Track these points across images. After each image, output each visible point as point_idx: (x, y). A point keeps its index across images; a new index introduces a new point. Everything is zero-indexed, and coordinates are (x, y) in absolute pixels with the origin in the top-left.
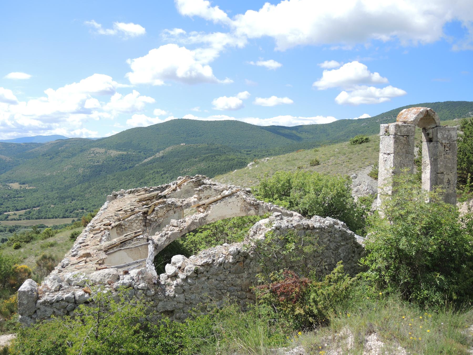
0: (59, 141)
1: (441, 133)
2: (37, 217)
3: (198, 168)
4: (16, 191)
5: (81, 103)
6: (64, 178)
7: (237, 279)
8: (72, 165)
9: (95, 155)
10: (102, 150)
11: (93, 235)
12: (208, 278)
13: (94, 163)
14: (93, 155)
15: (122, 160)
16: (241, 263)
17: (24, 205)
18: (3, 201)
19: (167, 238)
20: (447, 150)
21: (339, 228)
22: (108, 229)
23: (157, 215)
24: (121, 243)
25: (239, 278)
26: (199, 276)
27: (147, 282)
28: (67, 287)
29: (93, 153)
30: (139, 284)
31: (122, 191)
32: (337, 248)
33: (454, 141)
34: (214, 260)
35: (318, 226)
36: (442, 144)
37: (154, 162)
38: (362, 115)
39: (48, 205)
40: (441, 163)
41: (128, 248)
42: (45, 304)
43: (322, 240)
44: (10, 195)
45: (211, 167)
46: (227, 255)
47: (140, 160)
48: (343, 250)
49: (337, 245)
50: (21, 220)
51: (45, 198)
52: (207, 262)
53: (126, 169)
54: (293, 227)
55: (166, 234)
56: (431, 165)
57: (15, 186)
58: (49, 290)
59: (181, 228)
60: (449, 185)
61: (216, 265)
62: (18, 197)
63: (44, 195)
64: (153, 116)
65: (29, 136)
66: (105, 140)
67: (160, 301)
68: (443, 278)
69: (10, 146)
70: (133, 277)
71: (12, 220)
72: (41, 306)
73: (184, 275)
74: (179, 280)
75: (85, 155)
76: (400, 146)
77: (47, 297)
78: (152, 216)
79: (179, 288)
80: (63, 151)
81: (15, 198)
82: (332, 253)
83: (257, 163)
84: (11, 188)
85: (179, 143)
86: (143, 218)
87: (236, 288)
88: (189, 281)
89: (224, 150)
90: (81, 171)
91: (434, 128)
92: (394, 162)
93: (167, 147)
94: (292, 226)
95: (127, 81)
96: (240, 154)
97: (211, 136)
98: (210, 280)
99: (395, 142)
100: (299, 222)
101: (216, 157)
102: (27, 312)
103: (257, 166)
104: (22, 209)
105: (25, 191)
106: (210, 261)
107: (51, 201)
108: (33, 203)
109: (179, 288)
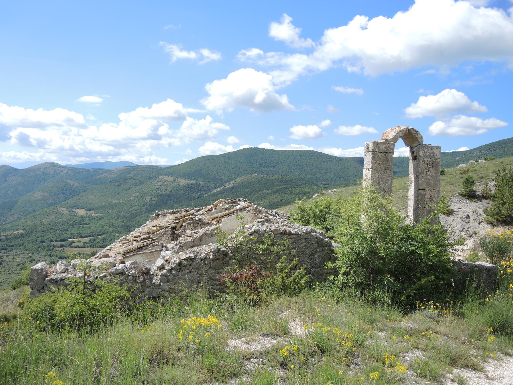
0: (127, 168)
1: (423, 151)
2: (101, 245)
3: (270, 201)
4: (82, 217)
5: (152, 128)
6: (130, 206)
7: (216, 274)
8: (140, 193)
9: (163, 183)
10: (171, 179)
11: (121, 244)
12: (191, 272)
13: (161, 191)
14: (161, 183)
15: (190, 189)
16: (221, 260)
17: (89, 232)
18: (68, 227)
19: (180, 247)
20: (429, 168)
21: (316, 235)
22: (138, 241)
23: (185, 230)
24: (138, 248)
25: (218, 273)
26: (182, 268)
27: (138, 271)
28: (72, 270)
29: (162, 181)
30: (131, 272)
31: (165, 211)
32: (313, 254)
33: (437, 159)
34: (197, 256)
35: (295, 232)
36: (424, 161)
37: (224, 193)
38: (458, 149)
39: (113, 234)
40: (423, 180)
41: (144, 253)
42: (51, 281)
43: (298, 246)
44: (76, 222)
45: (283, 200)
46: (209, 252)
47: (209, 190)
48: (319, 256)
49: (312, 251)
50: (85, 247)
51: (110, 226)
52: (190, 256)
53: (194, 199)
54: (271, 231)
55: (180, 243)
56: (415, 182)
57: (82, 212)
58: (57, 272)
59: (194, 238)
61: (198, 260)
62: (84, 224)
63: (110, 223)
64: (226, 144)
65: (98, 161)
66: (174, 168)
67: (148, 287)
68: (392, 280)
69: (79, 171)
70: (127, 266)
71: (76, 247)
72: (48, 283)
73: (170, 267)
74: (165, 271)
75: (153, 183)
76: (378, 162)
77: (54, 276)
78: (180, 231)
79: (164, 277)
80: (131, 178)
81: (80, 224)
82: (308, 258)
83: (323, 194)
84: (77, 214)
85: (251, 174)
86: (171, 233)
87: (215, 282)
88: (173, 272)
89: (299, 182)
90: (148, 199)
91: (417, 146)
92: (372, 177)
93: (238, 177)
94: (269, 230)
95: (203, 107)
96: (316, 187)
97: (286, 167)
98: (192, 273)
99: (373, 158)
100: (277, 227)
101: (290, 189)
102: (37, 287)
103: (322, 197)
104: (87, 237)
105: (91, 218)
106: (193, 256)
107: (116, 230)
108: (98, 231)
109: (164, 277)
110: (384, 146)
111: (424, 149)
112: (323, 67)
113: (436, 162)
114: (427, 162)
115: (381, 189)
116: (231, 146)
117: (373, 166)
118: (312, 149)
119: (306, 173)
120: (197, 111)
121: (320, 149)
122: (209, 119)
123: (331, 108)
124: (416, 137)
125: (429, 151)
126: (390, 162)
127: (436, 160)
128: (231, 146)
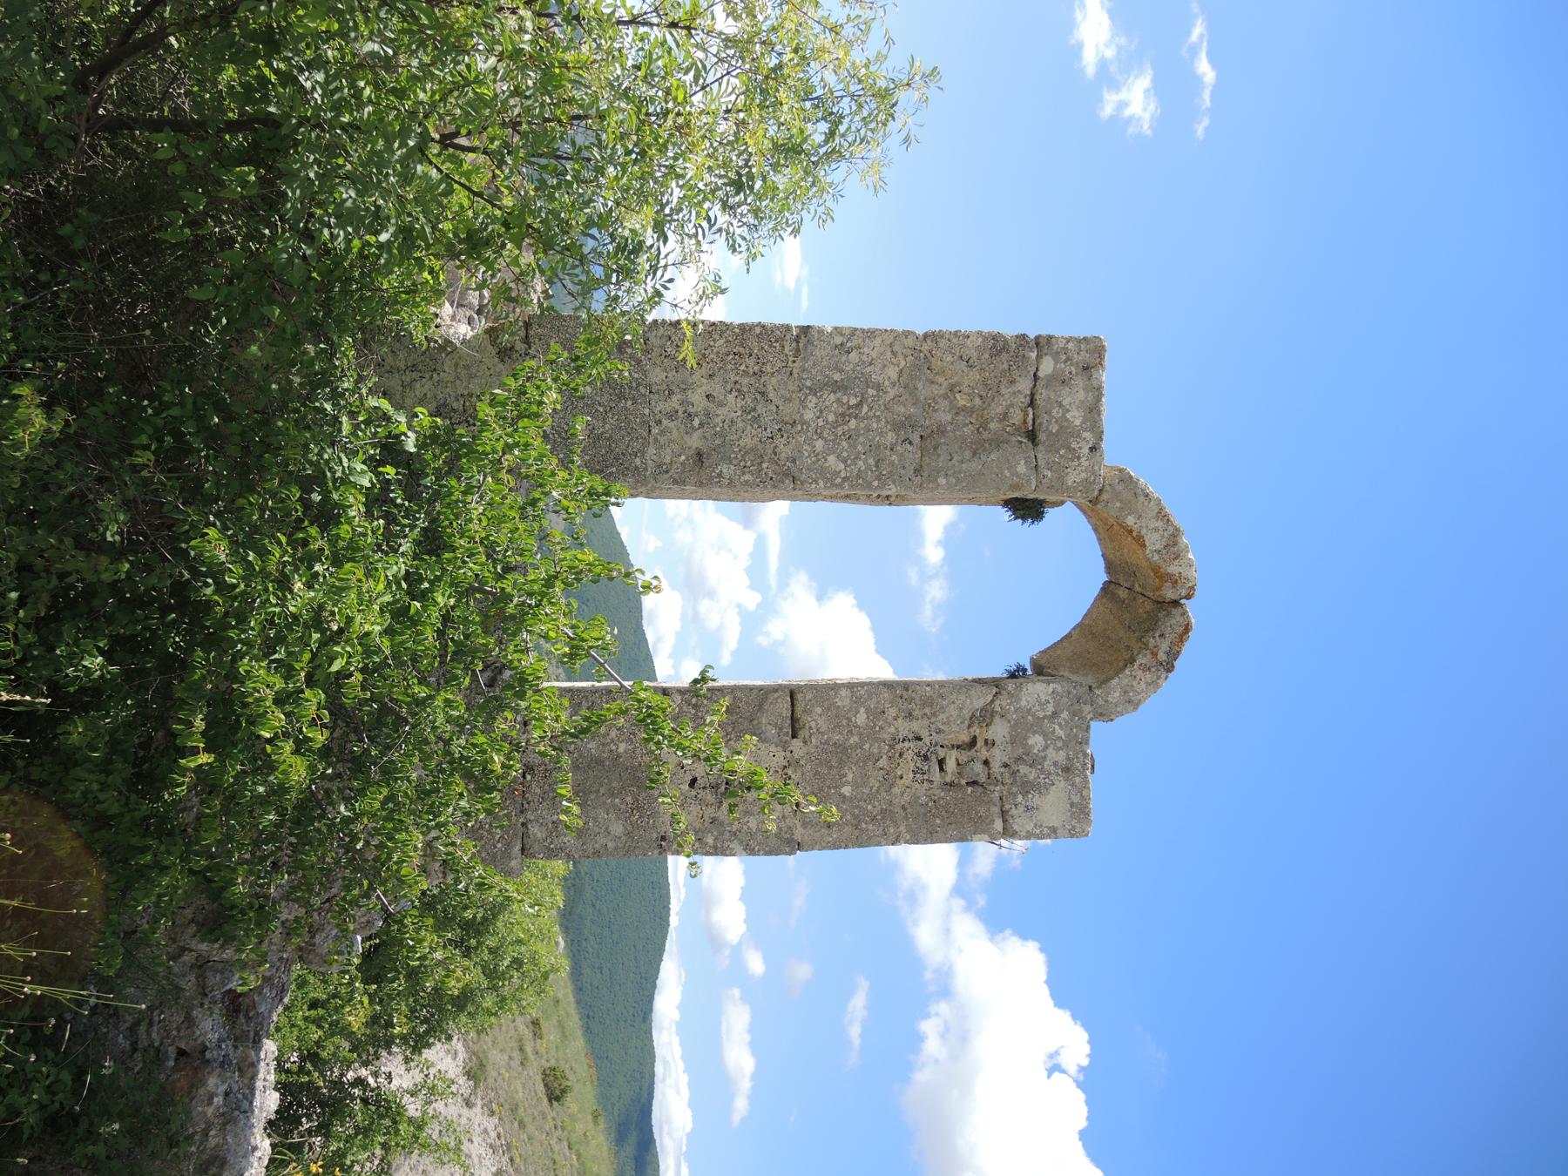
1: (1050, 709)
20: (941, 763)
33: (1004, 814)
40: (861, 718)
60: (714, 787)
76: (974, 376)
110: (1076, 417)
111: (1065, 715)
112: (925, 935)
113: (982, 811)
114: (980, 743)
115: (788, 400)
116: (672, 672)
117: (943, 343)
118: (674, 920)
119: (598, 907)
120: (773, 563)
121: (674, 949)
122: (752, 600)
123: (803, 971)
124: (1132, 661)
125: (1051, 753)
126: (975, 465)
127: (996, 810)
128: (672, 672)
